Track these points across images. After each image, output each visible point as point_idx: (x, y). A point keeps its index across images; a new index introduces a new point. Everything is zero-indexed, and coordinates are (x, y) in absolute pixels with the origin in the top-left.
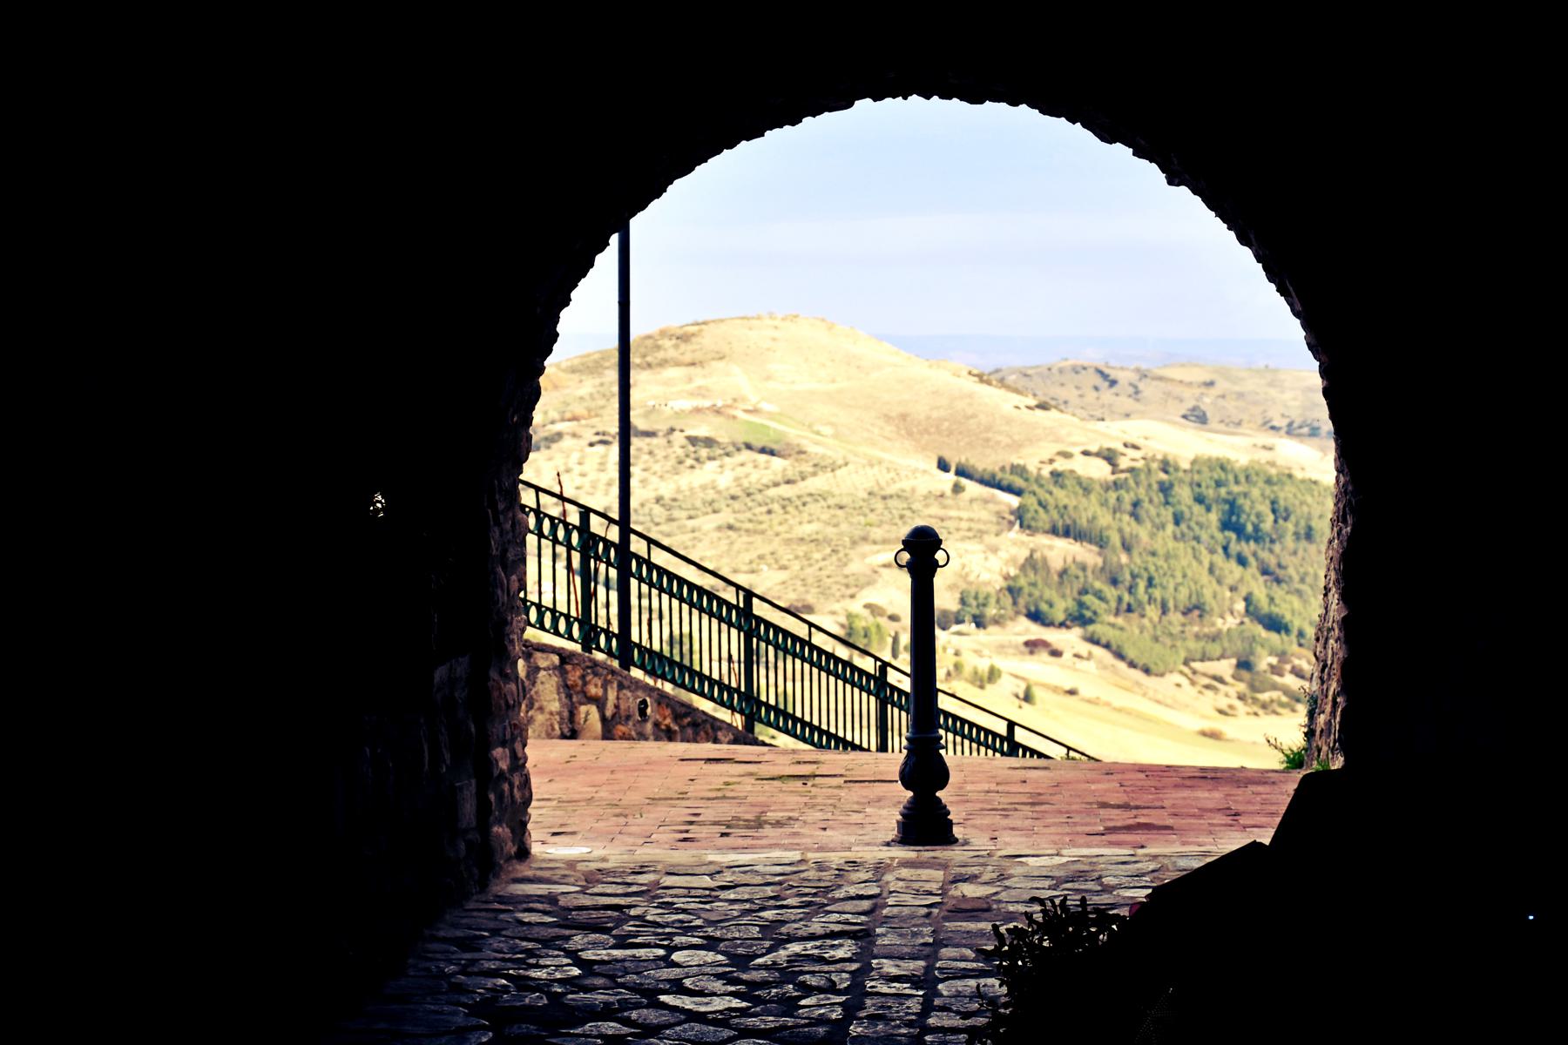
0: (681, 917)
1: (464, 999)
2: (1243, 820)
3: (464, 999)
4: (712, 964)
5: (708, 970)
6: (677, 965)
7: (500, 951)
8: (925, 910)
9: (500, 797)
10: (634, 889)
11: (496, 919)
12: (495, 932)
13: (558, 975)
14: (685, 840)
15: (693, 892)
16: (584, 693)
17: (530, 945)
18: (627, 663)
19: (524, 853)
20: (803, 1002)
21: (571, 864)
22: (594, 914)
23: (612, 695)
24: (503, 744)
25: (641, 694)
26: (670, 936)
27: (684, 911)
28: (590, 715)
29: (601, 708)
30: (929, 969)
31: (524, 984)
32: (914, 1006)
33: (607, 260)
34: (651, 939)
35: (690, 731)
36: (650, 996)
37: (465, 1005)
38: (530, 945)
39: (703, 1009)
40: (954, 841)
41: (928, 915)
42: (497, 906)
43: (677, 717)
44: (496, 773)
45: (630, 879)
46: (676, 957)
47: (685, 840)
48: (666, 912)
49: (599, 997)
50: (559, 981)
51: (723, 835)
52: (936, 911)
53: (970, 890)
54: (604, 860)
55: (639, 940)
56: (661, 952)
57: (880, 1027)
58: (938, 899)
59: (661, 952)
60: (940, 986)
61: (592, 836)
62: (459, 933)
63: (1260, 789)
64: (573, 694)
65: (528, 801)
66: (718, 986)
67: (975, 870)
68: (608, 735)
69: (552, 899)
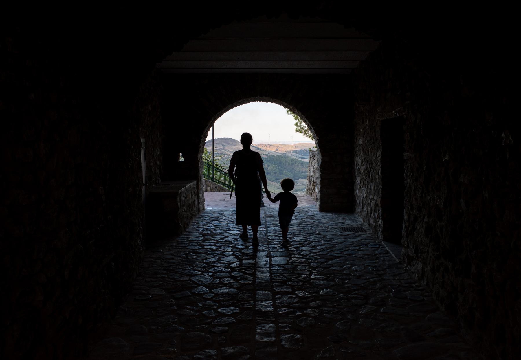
0: (228, 218)
1: (198, 232)
2: (303, 202)
3: (198, 232)
4: (234, 226)
5: (233, 227)
6: (229, 226)
7: (202, 224)
8: (263, 217)
9: (201, 201)
10: (220, 214)
11: (201, 219)
12: (201, 221)
13: (211, 228)
14: (226, 206)
15: (229, 215)
16: (208, 185)
17: (206, 223)
18: (214, 181)
19: (204, 209)
20: (249, 232)
21: (211, 210)
22: (215, 218)
23: (212, 186)
24: (201, 193)
25: (216, 185)
26: (227, 221)
27: (228, 217)
28: (209, 188)
29: (210, 188)
30: (266, 226)
31: (207, 230)
32: (265, 232)
33: (211, 129)
34: (224, 222)
35: (222, 190)
36: (226, 231)
37: (198, 233)
38: (206, 223)
39: (234, 233)
40: (265, 206)
41: (263, 217)
42: (201, 217)
43: (220, 188)
44: (200, 198)
45: (220, 213)
46: (228, 225)
47: (226, 206)
48: (319, 253)
49: (218, 232)
50: (212, 229)
51: (231, 206)
52: (264, 217)
53: (269, 214)
54: (215, 210)
55: (222, 222)
56: (226, 224)
57: (261, 235)
58: (264, 215)
59: (226, 224)
60: (268, 229)
61: (212, 206)
62: (196, 221)
63: (303, 197)
64: (207, 186)
65: (204, 202)
66: (235, 229)
67: (269, 211)
68: (211, 191)
69: (209, 216)
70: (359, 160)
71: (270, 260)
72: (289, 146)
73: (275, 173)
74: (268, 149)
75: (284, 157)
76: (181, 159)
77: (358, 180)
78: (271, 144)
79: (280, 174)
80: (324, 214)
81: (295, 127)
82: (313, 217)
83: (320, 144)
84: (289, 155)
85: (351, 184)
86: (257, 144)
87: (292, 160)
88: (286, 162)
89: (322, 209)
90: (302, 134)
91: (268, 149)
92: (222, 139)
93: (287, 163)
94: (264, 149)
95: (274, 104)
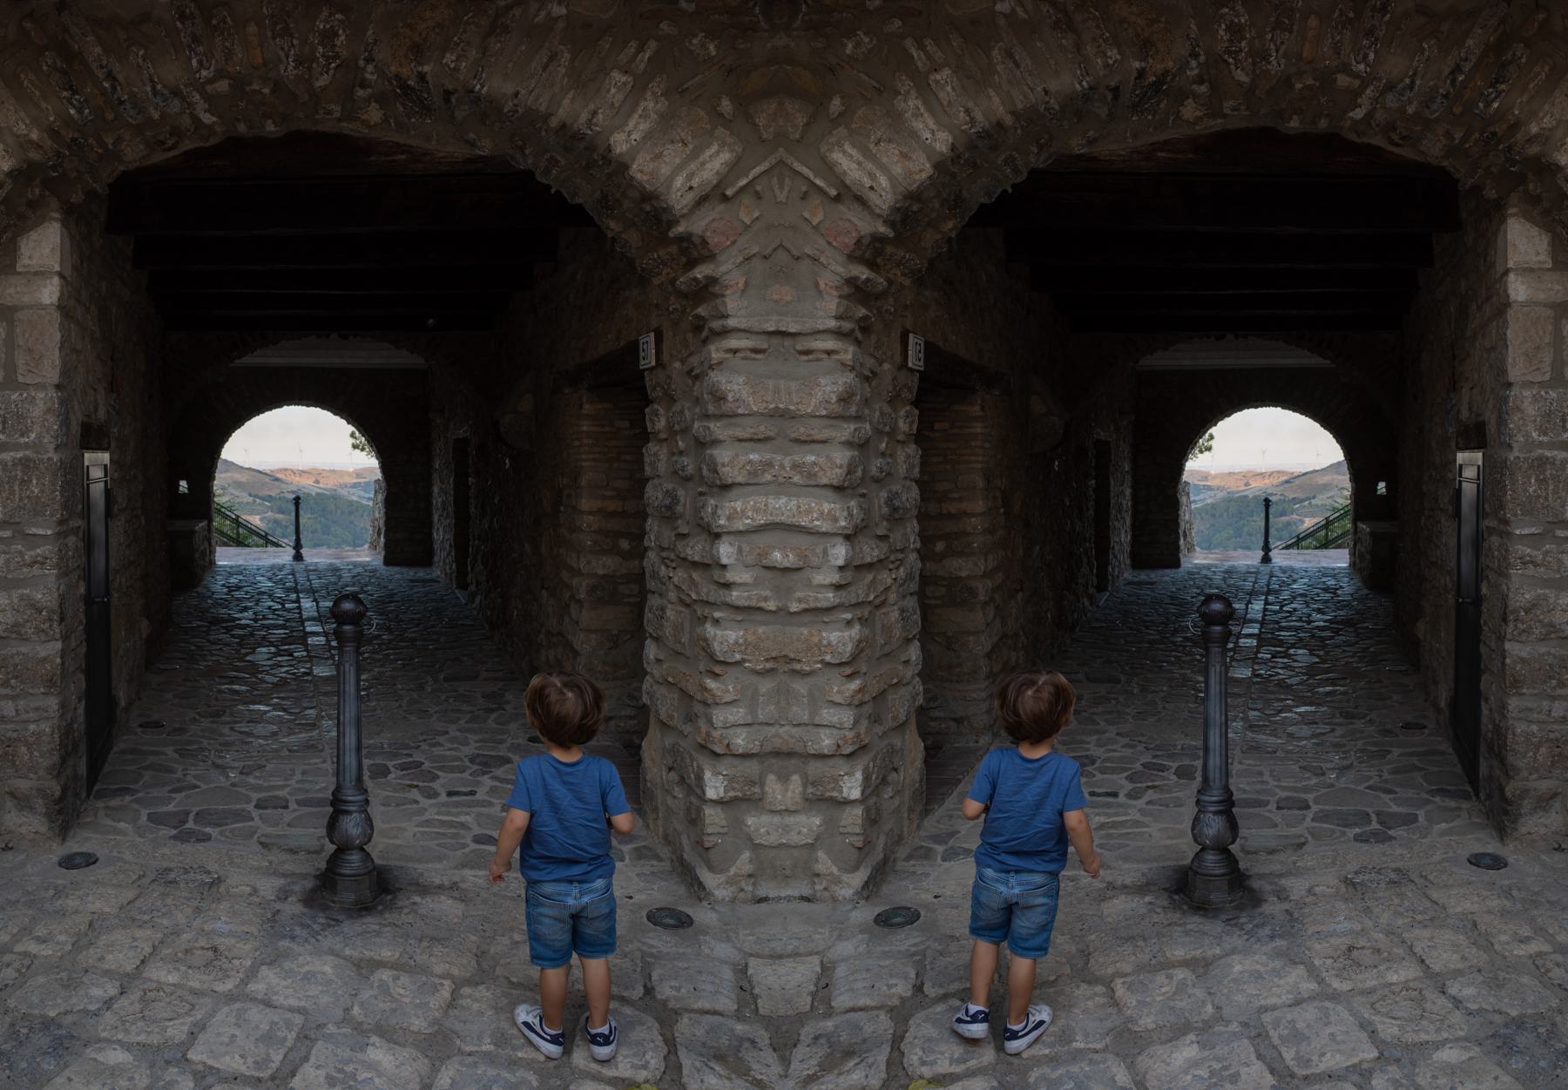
70: (436, 490)
71: (317, 605)
72: (342, 473)
73: (314, 532)
74: (297, 479)
75: (333, 497)
76: (183, 483)
77: (436, 518)
78: (305, 468)
79: (324, 534)
80: (390, 568)
81: (352, 441)
82: (374, 571)
83: (384, 467)
84: (344, 492)
85: (429, 524)
86: (272, 468)
87: (351, 503)
88: (337, 508)
89: (388, 562)
90: (364, 453)
91: (297, 479)
92: (1332, 465)
93: (339, 512)
94: (289, 479)
95: (318, 410)
